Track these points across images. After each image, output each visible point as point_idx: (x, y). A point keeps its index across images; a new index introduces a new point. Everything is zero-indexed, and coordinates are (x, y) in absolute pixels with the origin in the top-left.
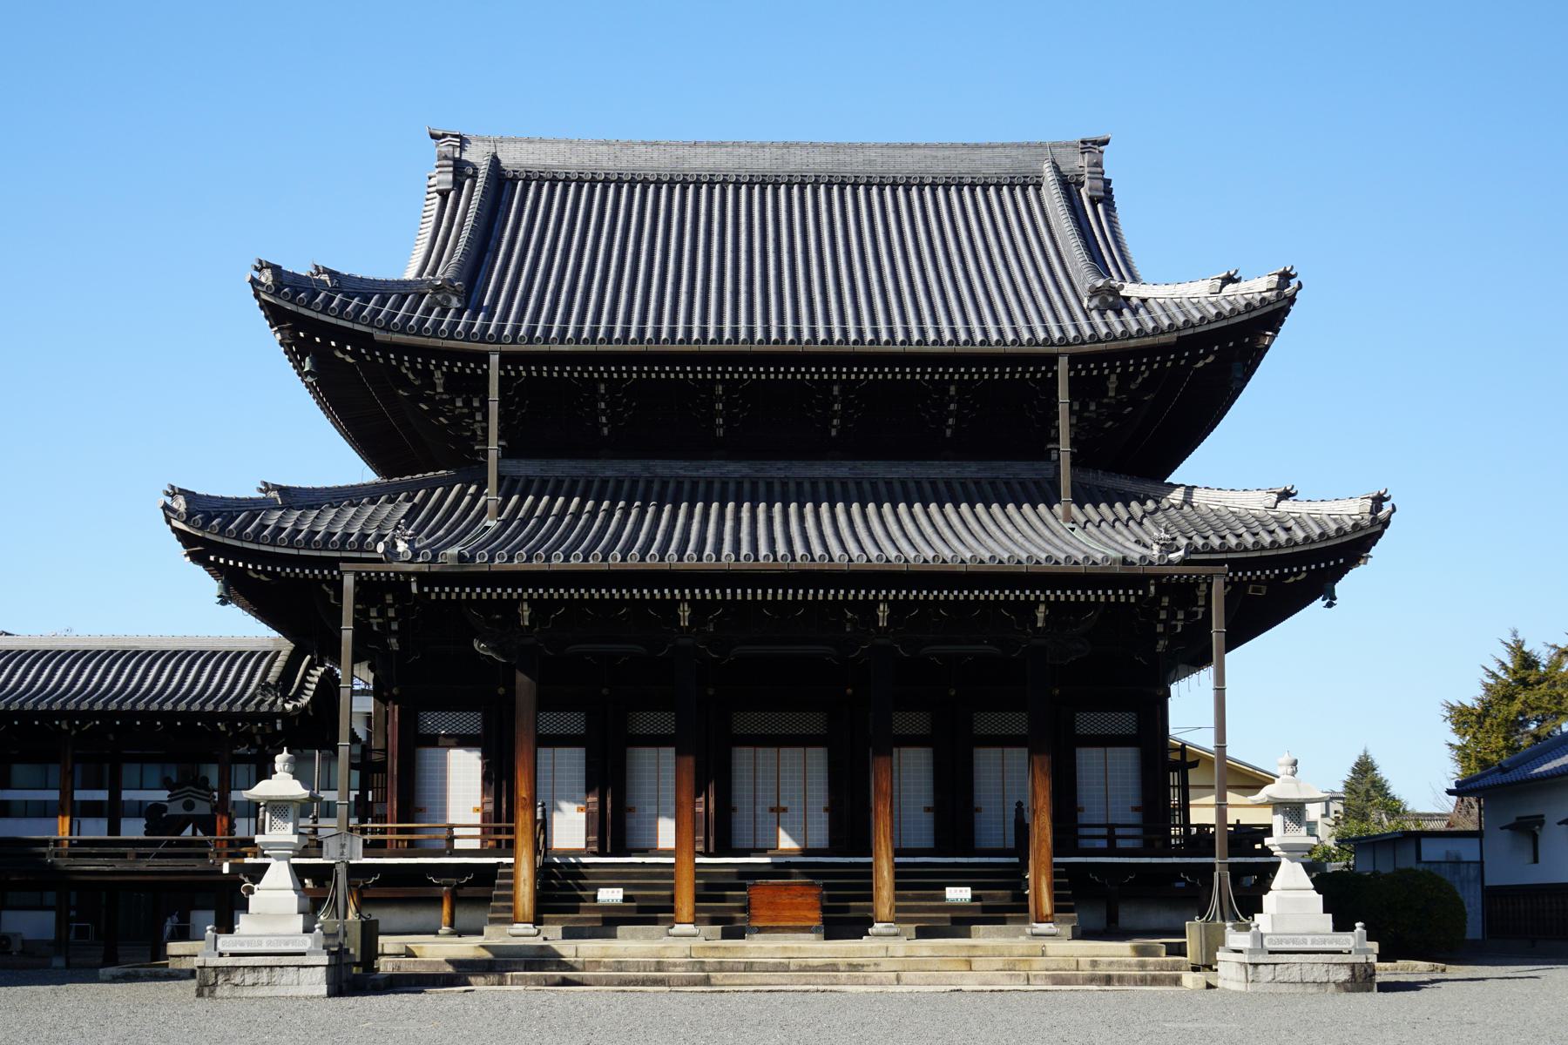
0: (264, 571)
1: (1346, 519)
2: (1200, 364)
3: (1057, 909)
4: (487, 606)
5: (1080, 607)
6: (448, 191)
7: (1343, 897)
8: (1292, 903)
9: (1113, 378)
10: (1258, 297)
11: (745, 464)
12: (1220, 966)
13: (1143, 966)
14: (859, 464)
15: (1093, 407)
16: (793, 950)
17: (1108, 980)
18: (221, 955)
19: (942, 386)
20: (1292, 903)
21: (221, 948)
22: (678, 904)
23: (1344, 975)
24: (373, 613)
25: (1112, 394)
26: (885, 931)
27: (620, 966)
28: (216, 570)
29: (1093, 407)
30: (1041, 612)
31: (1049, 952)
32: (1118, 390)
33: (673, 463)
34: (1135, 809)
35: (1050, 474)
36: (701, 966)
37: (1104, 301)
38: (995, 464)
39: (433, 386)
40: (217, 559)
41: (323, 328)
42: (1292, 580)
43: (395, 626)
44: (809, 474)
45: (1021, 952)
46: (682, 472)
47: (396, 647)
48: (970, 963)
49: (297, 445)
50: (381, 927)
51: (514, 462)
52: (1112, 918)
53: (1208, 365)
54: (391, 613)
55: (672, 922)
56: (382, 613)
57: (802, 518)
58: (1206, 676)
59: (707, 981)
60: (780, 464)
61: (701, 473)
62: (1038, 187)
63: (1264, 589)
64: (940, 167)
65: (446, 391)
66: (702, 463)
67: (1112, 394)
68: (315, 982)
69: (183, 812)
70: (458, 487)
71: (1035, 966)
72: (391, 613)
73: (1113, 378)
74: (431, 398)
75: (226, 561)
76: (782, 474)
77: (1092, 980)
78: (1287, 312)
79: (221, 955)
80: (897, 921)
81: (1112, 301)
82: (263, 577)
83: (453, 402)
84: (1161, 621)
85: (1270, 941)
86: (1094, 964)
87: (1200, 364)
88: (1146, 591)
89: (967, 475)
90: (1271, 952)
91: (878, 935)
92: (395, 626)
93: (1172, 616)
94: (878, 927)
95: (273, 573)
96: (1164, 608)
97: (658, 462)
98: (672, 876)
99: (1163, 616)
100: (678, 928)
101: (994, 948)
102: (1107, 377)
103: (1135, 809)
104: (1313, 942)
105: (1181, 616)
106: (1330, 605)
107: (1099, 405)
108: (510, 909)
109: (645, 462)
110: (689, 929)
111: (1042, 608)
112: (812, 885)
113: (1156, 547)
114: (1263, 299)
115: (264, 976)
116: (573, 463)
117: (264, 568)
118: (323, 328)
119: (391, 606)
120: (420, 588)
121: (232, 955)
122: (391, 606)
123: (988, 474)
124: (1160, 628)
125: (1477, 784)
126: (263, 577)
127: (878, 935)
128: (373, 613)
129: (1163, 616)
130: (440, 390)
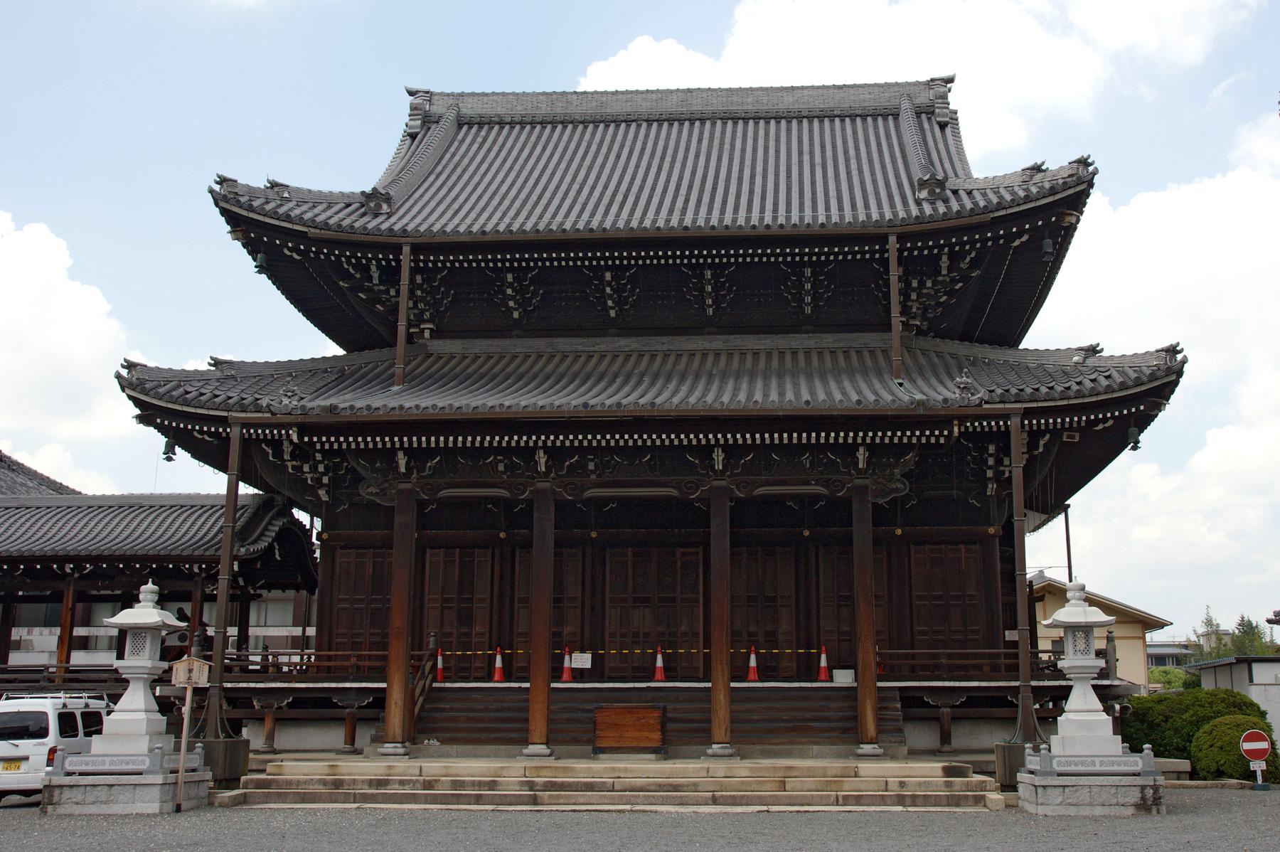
0: (209, 433)
1: (1145, 369)
2: (1017, 243)
3: (880, 731)
4: (370, 455)
5: (900, 450)
6: (417, 134)
7: (1136, 723)
8: (1084, 727)
9: (945, 258)
10: (1061, 182)
11: (634, 339)
12: (1020, 787)
13: (948, 784)
14: (731, 337)
15: (929, 284)
16: (619, 770)
17: (914, 801)
18: (69, 774)
19: (797, 267)
20: (1084, 727)
21: (69, 768)
22: (715, 726)
23: (1135, 796)
24: (306, 468)
25: (944, 272)
26: (720, 752)
27: (457, 784)
28: (162, 429)
29: (929, 284)
30: (861, 454)
31: (861, 773)
32: (950, 269)
33: (573, 340)
36: (531, 786)
37: (931, 193)
38: (848, 335)
39: (370, 279)
40: (163, 422)
41: (282, 239)
42: (1100, 427)
43: (325, 480)
44: (689, 347)
45: (834, 772)
46: (580, 348)
47: (325, 498)
48: (784, 782)
49: (278, 332)
50: (252, 748)
51: (440, 342)
52: (946, 738)
54: (321, 468)
56: (314, 469)
58: (1062, 517)
59: (534, 801)
60: (664, 339)
61: (596, 348)
62: (896, 116)
65: (381, 282)
66: (598, 340)
67: (944, 272)
68: (150, 803)
69: (178, 643)
71: (846, 787)
72: (321, 468)
73: (945, 258)
75: (170, 423)
76: (665, 347)
77: (900, 800)
78: (1088, 195)
79: (69, 774)
81: (936, 186)
82: (206, 438)
83: (387, 292)
84: (990, 467)
85: (1059, 764)
86: (902, 784)
87: (1017, 243)
88: (951, 432)
89: (824, 345)
90: (1059, 775)
91: (714, 756)
92: (325, 480)
95: (217, 434)
96: (991, 455)
97: (561, 340)
99: (991, 462)
100: (532, 749)
101: (809, 768)
102: (939, 257)
104: (1102, 764)
106: (1135, 448)
107: (935, 283)
109: (549, 340)
110: (542, 749)
111: (861, 450)
113: (957, 391)
114: (1065, 183)
115: (102, 794)
116: (489, 342)
117: (201, 428)
118: (282, 239)
119: (320, 462)
120: (300, 437)
121: (81, 774)
122: (320, 462)
123: (842, 345)
124: (990, 474)
126: (206, 438)
127: (714, 756)
128: (306, 468)
129: (991, 462)
130: (376, 281)
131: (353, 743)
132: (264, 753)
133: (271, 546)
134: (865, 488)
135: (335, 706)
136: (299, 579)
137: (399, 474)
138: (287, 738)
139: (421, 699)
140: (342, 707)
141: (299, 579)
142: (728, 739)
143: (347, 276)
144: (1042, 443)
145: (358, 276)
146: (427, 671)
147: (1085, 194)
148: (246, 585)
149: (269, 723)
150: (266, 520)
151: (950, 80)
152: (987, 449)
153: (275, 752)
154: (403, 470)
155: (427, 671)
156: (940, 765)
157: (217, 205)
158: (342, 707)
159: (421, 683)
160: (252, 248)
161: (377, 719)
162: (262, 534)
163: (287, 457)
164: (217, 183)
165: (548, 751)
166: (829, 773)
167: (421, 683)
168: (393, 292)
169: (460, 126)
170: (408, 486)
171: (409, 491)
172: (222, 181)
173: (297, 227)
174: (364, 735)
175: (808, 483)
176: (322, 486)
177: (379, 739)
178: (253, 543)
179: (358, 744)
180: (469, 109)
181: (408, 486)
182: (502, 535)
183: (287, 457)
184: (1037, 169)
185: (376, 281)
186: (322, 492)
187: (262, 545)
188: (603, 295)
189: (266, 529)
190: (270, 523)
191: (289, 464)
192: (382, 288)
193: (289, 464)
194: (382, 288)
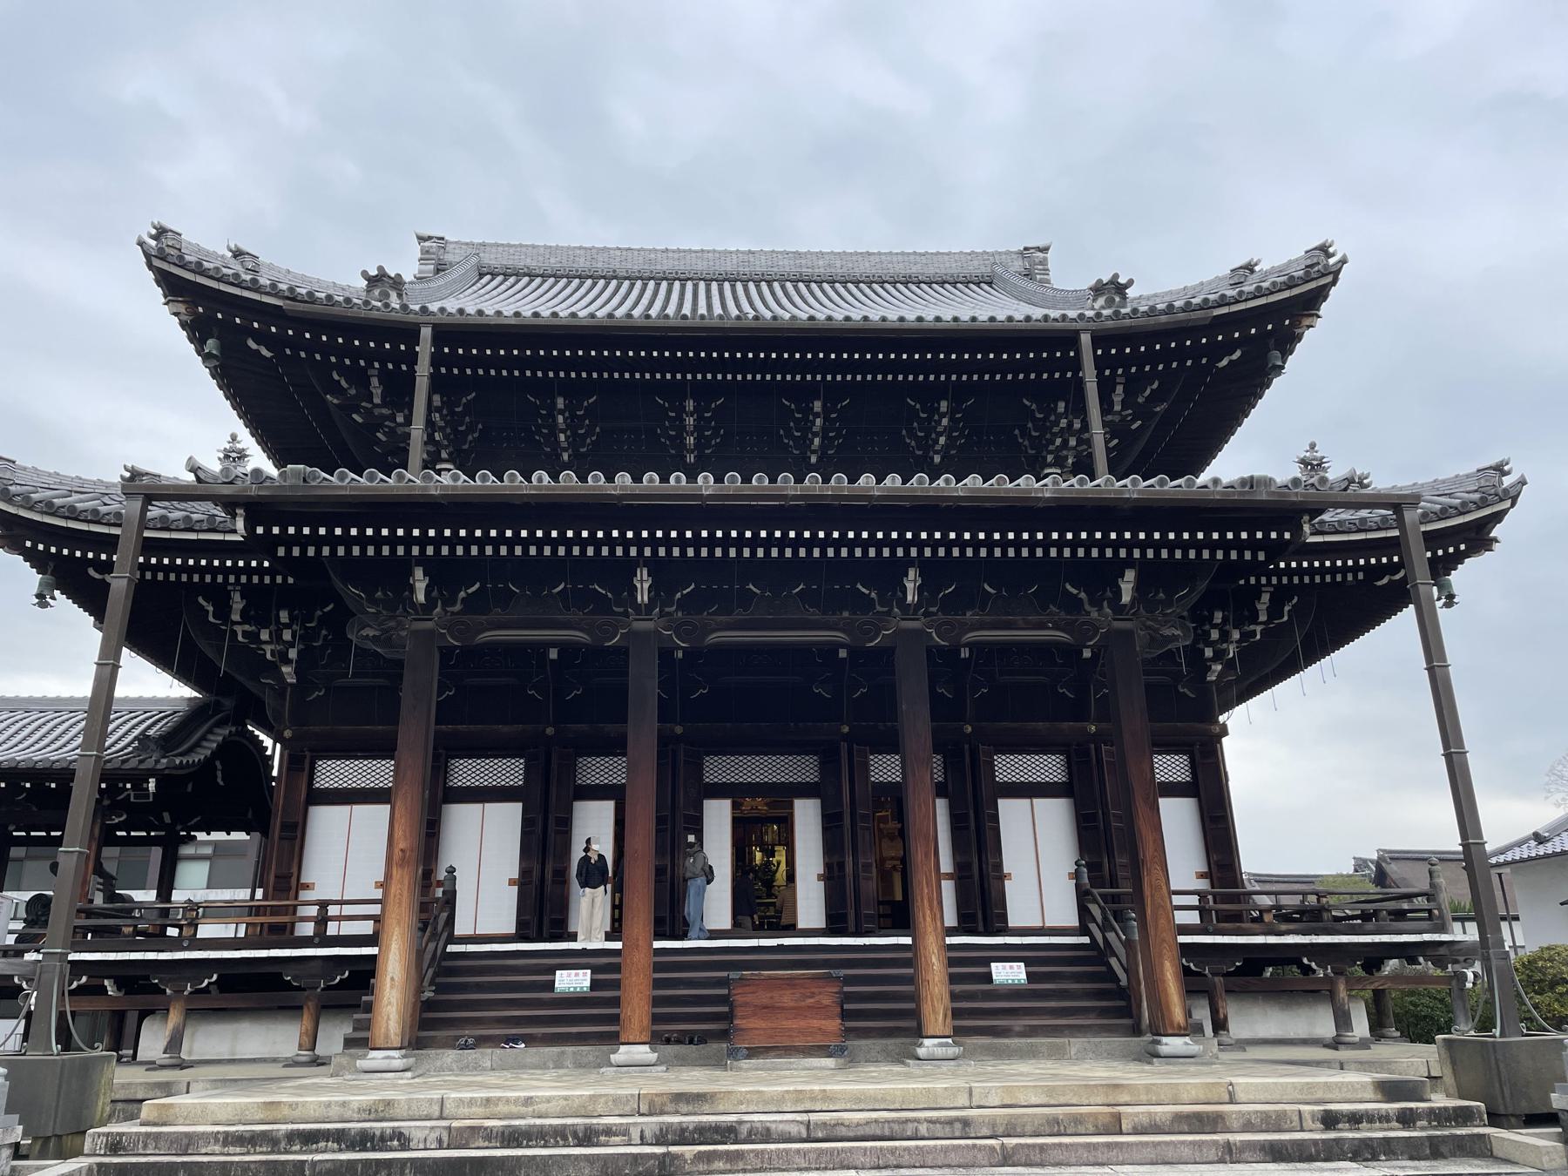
9: (1120, 389)
22: (926, 1009)
24: (265, 636)
25: (1117, 408)
26: (940, 1052)
34: (1201, 876)
35: (852, 928)
40: (35, 546)
43: (293, 654)
47: (292, 680)
53: (1243, 340)
54: (287, 635)
55: (614, 1039)
56: (276, 637)
57: (773, 294)
58: (1403, 624)
63: (1361, 576)
64: (900, 269)
65: (384, 404)
67: (1117, 408)
70: (252, 344)
72: (287, 635)
74: (369, 412)
80: (958, 1032)
92: (293, 654)
93: (1225, 637)
94: (928, 1046)
98: (616, 968)
100: (624, 1053)
103: (1201, 876)
105: (1236, 635)
108: (849, 997)
110: (643, 1052)
112: (828, 977)
118: (248, 333)
119: (287, 626)
125: (1509, 857)
128: (265, 636)
130: (377, 400)
131: (313, 1049)
132: (163, 1067)
133: (208, 764)
134: (1128, 635)
135: (288, 987)
136: (250, 815)
137: (413, 605)
138: (209, 1040)
139: (431, 972)
140: (299, 989)
141: (250, 815)
142: (949, 1031)
143: (336, 389)
144: (1287, 608)
145: (353, 392)
146: (440, 928)
147: (1320, 295)
148: (174, 823)
149: (175, 1017)
150: (205, 728)
151: (1045, 250)
152: (1212, 617)
153: (182, 1065)
154: (421, 597)
155: (440, 928)
156: (1366, 1078)
157: (150, 266)
158: (299, 989)
159: (1099, 918)
160: (197, 330)
161: (355, 1007)
162: (197, 745)
163: (236, 617)
164: (152, 237)
165: (653, 1057)
166: (1185, 1097)
167: (431, 946)
168: (400, 419)
169: (481, 276)
170: (429, 625)
171: (430, 633)
172: (161, 232)
173: (266, 299)
174: (333, 1036)
175: (1045, 627)
176: (288, 662)
177: (359, 1042)
178: (181, 755)
179: (319, 1051)
180: (489, 259)
181: (429, 625)
182: (550, 731)
183: (236, 617)
184: (1250, 268)
185: (377, 400)
186: (285, 669)
187: (198, 756)
188: (682, 428)
189: (203, 738)
190: (210, 731)
191: (239, 629)
192: (385, 411)
193: (239, 629)
194: (385, 411)
